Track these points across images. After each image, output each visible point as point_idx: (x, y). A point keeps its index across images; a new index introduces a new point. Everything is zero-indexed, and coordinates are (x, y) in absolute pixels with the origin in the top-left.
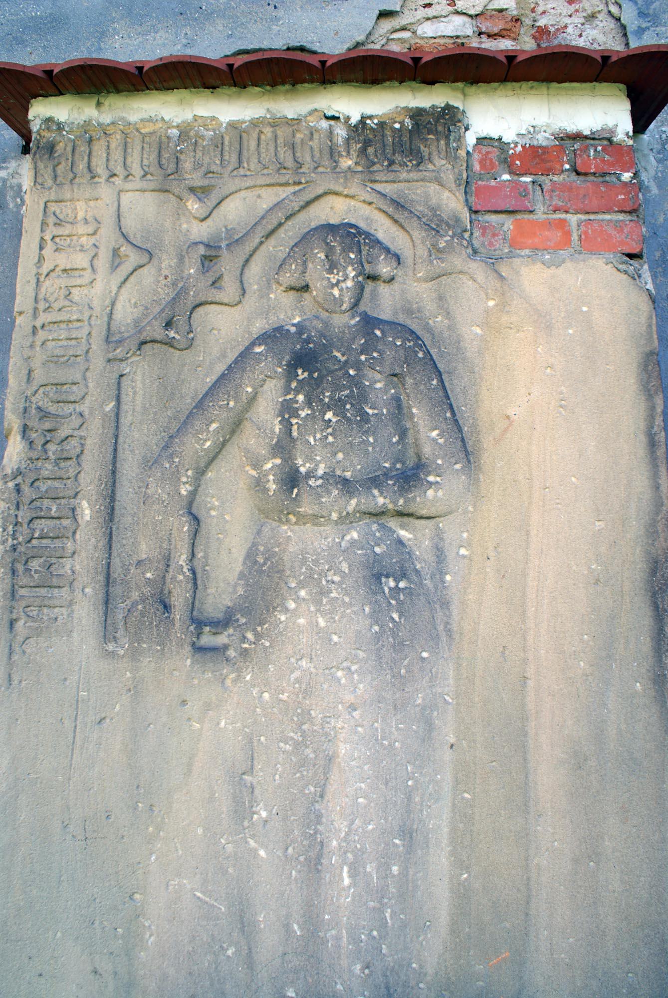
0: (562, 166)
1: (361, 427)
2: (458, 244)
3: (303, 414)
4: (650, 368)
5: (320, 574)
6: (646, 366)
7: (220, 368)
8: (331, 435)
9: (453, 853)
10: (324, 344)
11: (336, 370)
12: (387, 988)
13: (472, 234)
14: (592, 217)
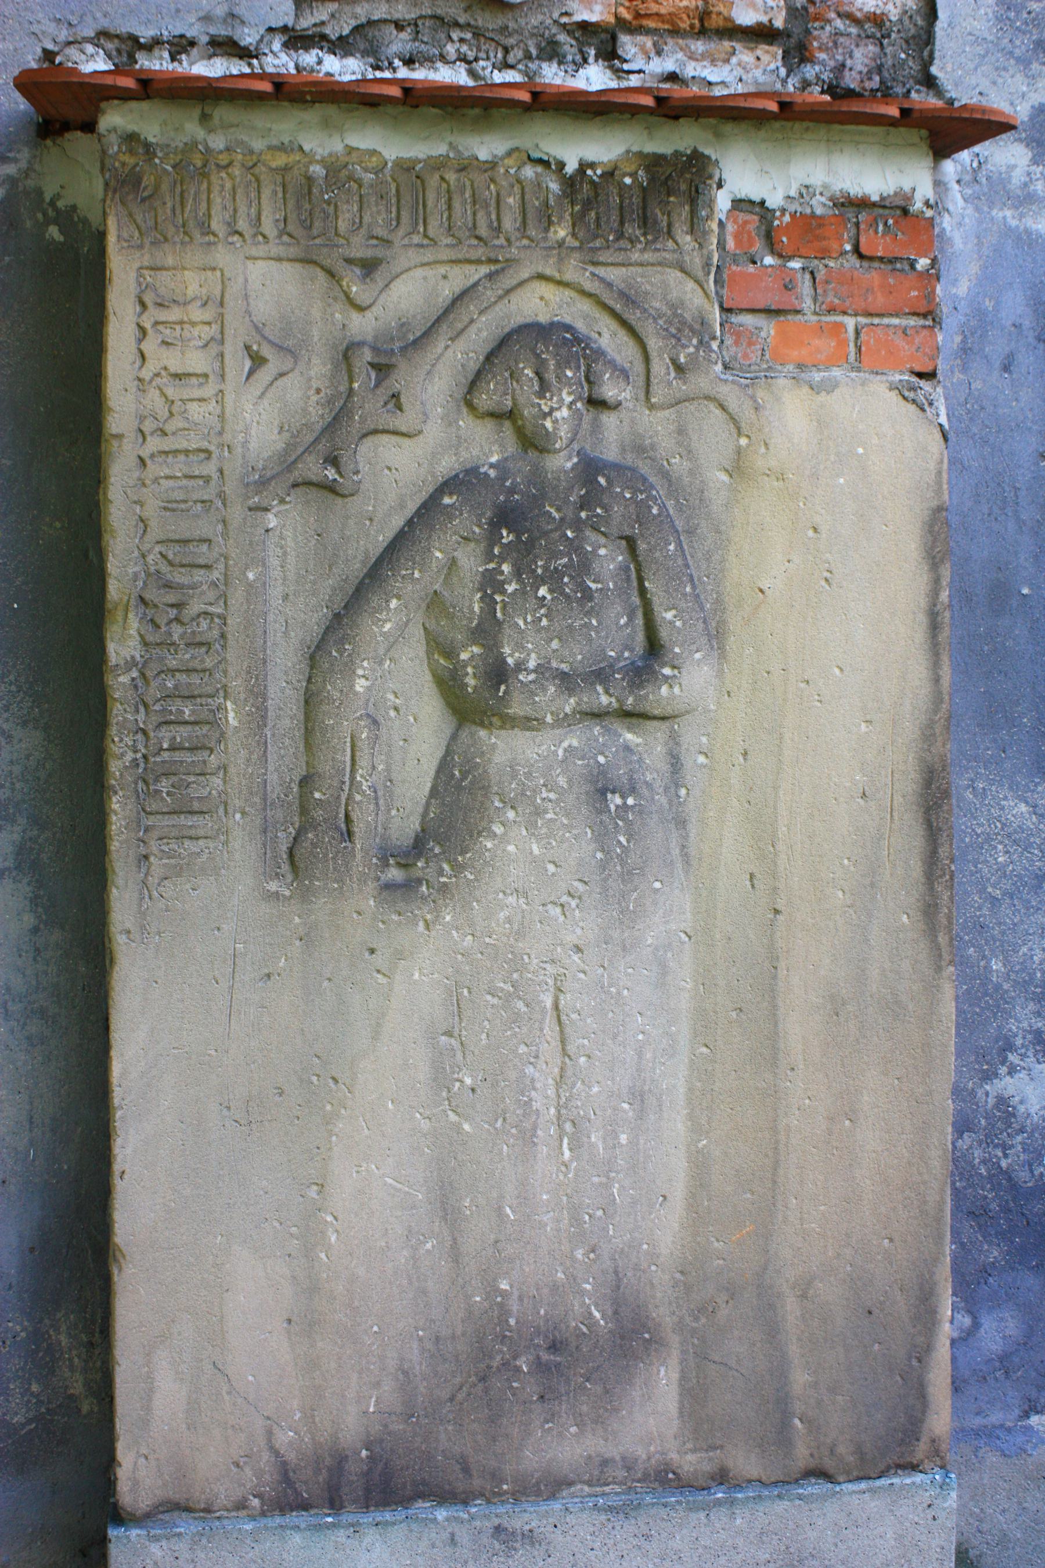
0: (842, 245)
1: (582, 606)
2: (704, 358)
3: (510, 588)
4: (936, 528)
5: (534, 791)
6: (931, 526)
7: (398, 522)
8: (546, 616)
9: (691, 1117)
10: (533, 495)
11: (552, 531)
12: (616, 1272)
13: (722, 342)
14: (876, 321)
